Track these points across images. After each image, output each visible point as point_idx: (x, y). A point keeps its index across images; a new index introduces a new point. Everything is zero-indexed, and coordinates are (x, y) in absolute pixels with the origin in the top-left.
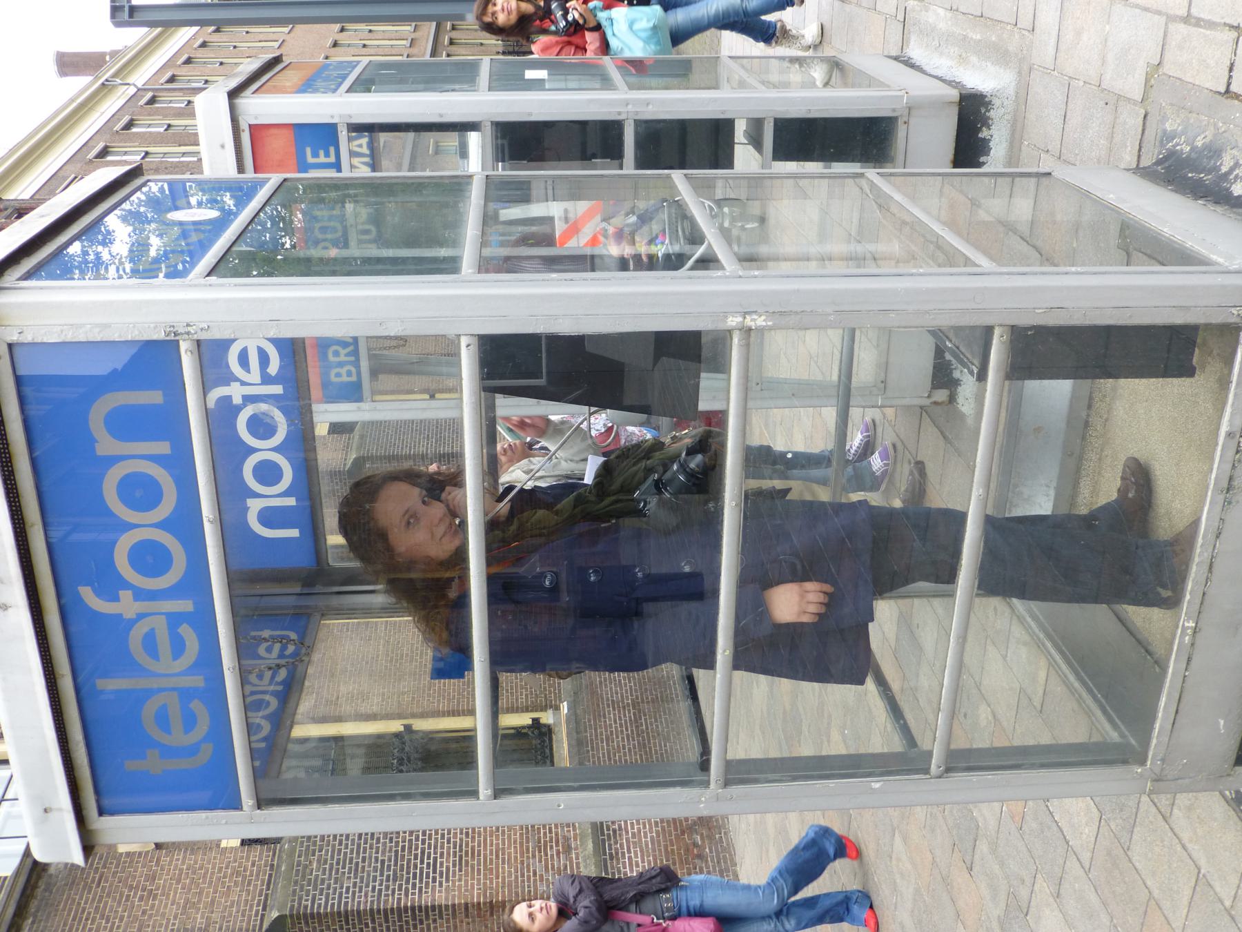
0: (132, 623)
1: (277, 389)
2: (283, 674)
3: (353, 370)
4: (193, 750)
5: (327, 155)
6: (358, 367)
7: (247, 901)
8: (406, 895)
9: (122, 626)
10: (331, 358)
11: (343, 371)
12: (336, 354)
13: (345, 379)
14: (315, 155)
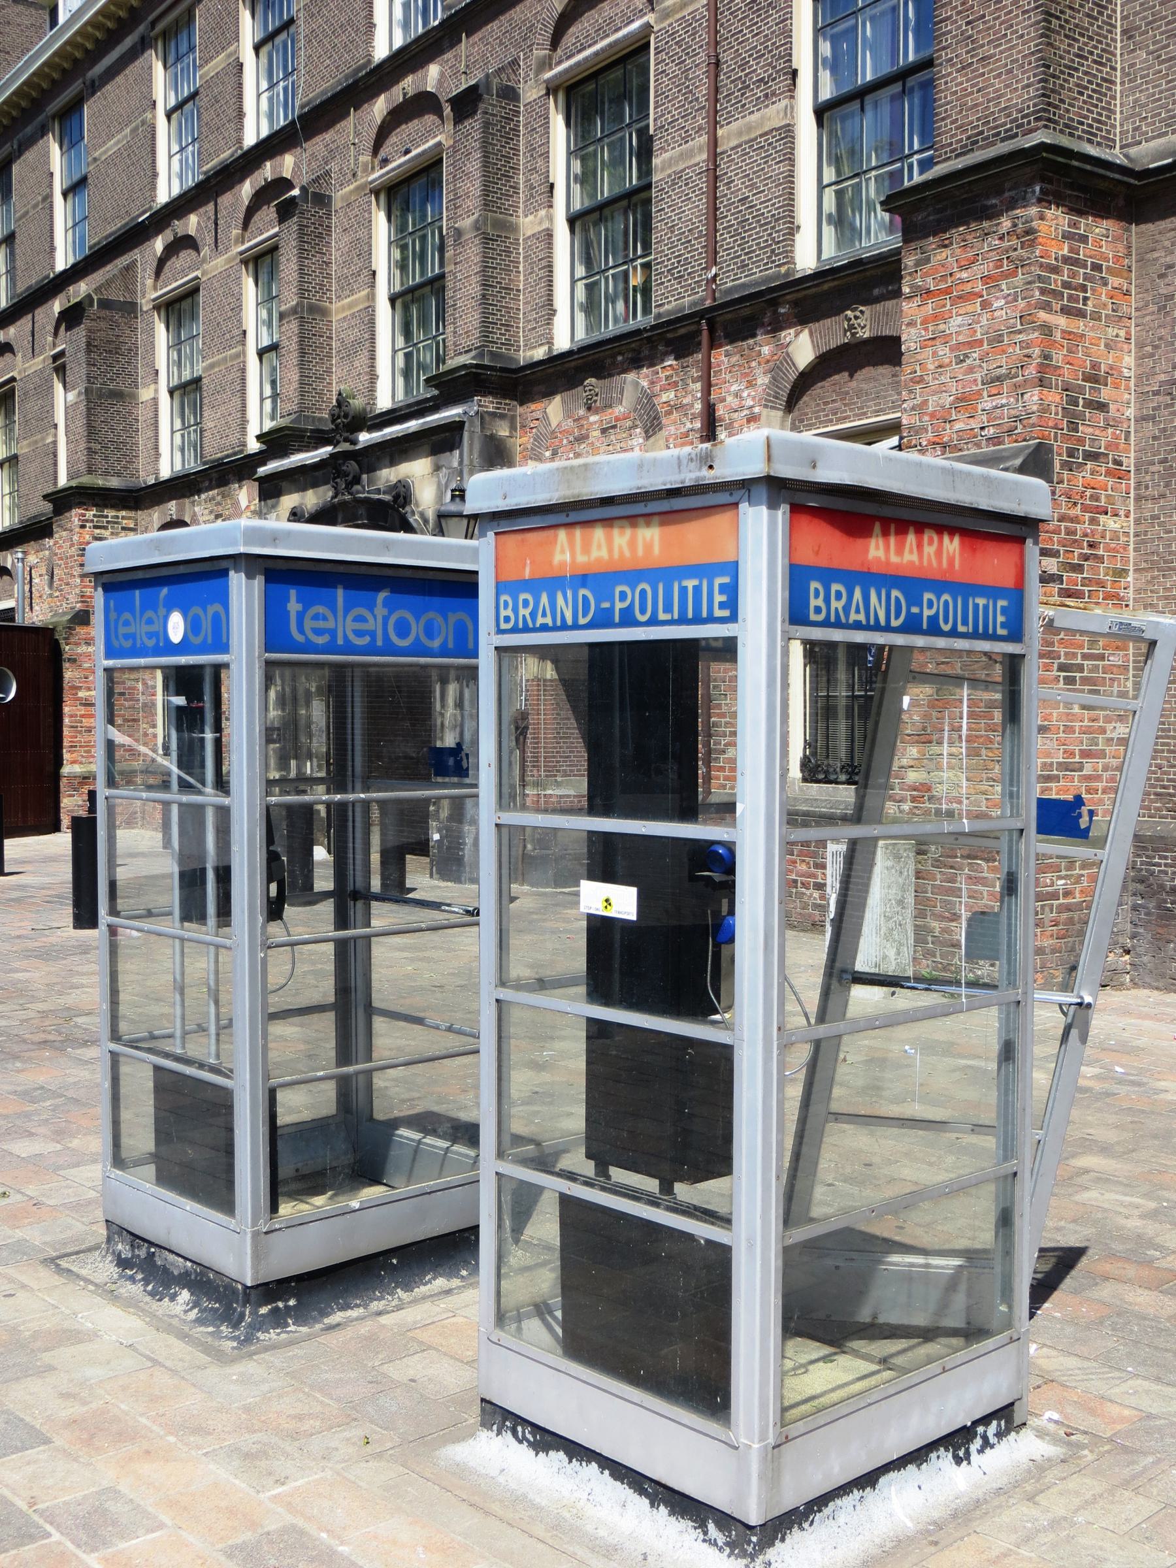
0: (156, 612)
4: (301, 630)
5: (1003, 625)
9: (371, 607)
10: (835, 587)
11: (820, 602)
13: (813, 603)
14: (723, 589)
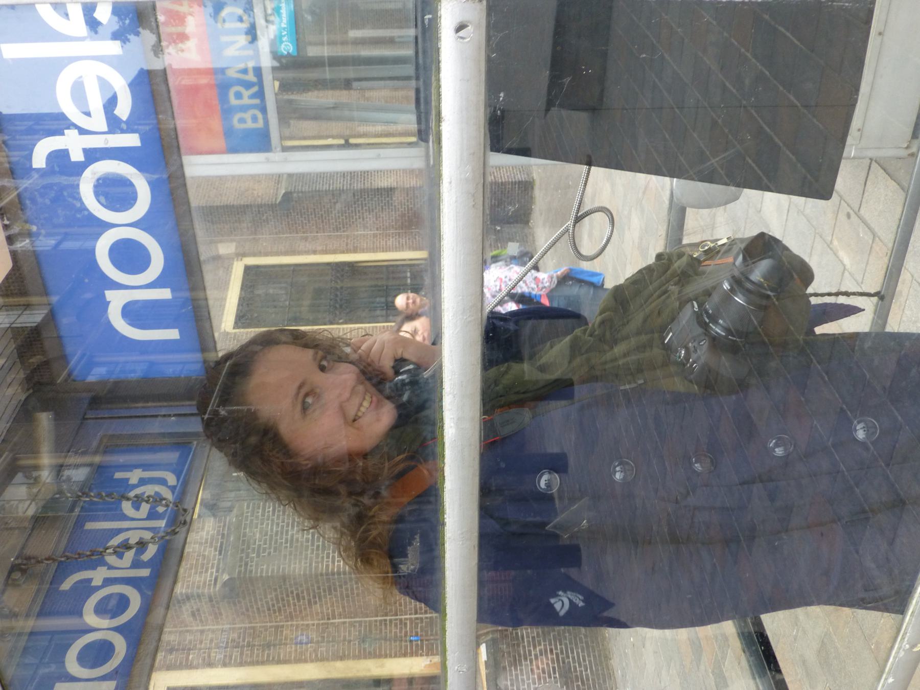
1: (132, 140)
2: (152, 550)
3: (260, 116)
6: (264, 110)
7: (203, 565)
8: (333, 562)
10: (233, 101)
11: (248, 116)
12: (239, 96)
13: (250, 125)
